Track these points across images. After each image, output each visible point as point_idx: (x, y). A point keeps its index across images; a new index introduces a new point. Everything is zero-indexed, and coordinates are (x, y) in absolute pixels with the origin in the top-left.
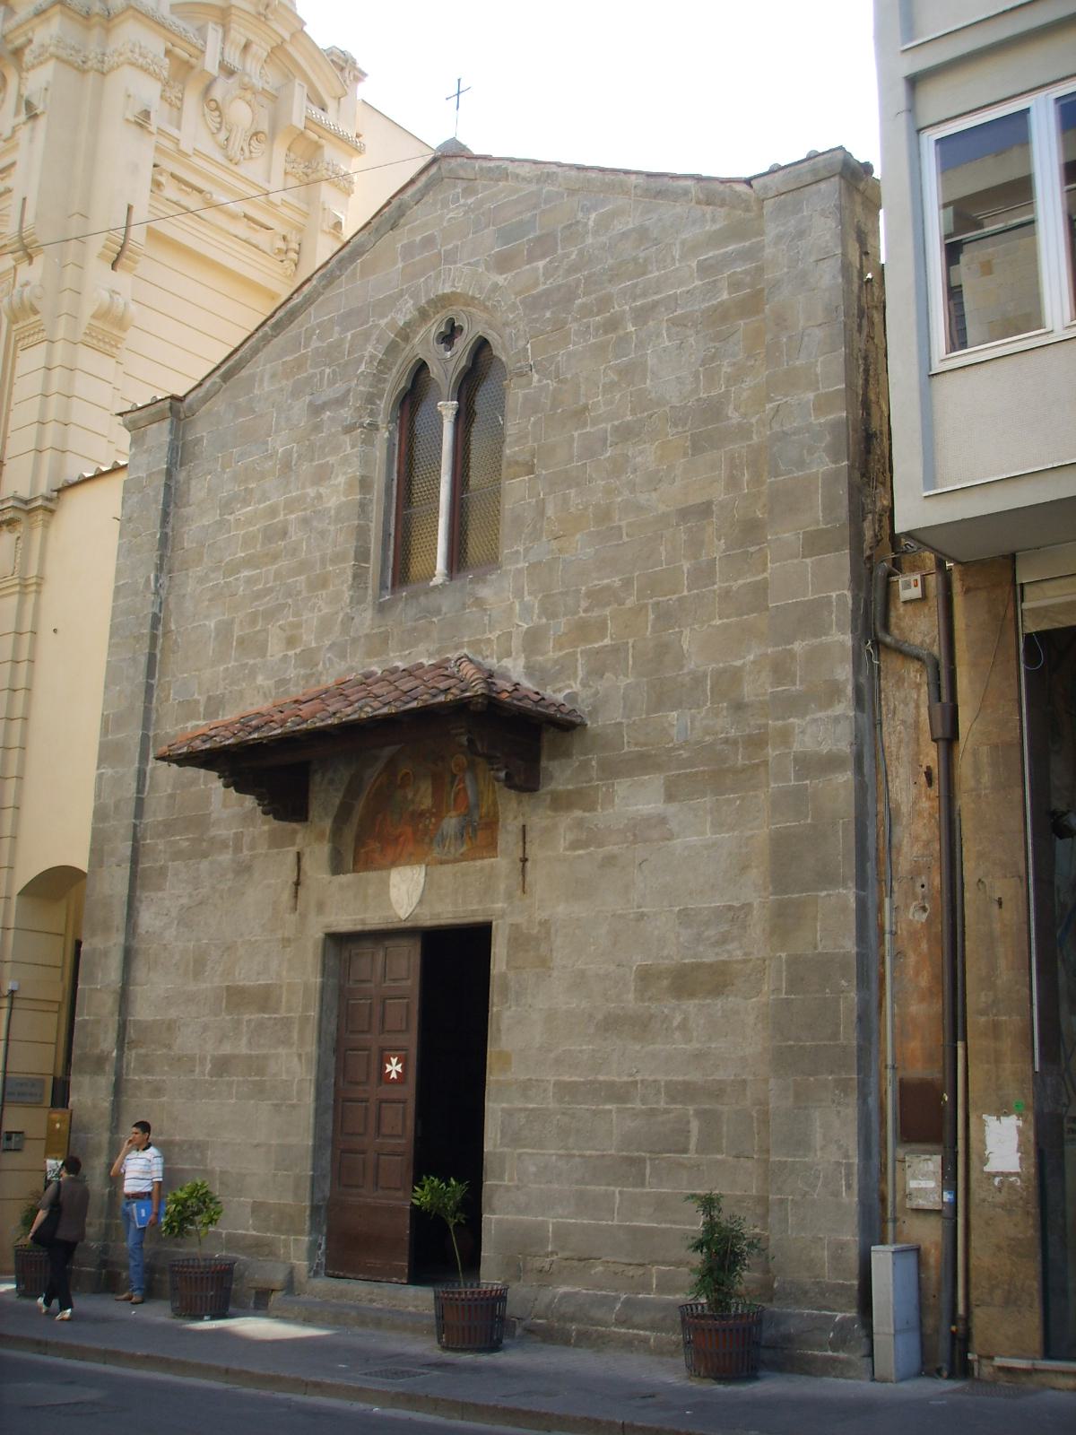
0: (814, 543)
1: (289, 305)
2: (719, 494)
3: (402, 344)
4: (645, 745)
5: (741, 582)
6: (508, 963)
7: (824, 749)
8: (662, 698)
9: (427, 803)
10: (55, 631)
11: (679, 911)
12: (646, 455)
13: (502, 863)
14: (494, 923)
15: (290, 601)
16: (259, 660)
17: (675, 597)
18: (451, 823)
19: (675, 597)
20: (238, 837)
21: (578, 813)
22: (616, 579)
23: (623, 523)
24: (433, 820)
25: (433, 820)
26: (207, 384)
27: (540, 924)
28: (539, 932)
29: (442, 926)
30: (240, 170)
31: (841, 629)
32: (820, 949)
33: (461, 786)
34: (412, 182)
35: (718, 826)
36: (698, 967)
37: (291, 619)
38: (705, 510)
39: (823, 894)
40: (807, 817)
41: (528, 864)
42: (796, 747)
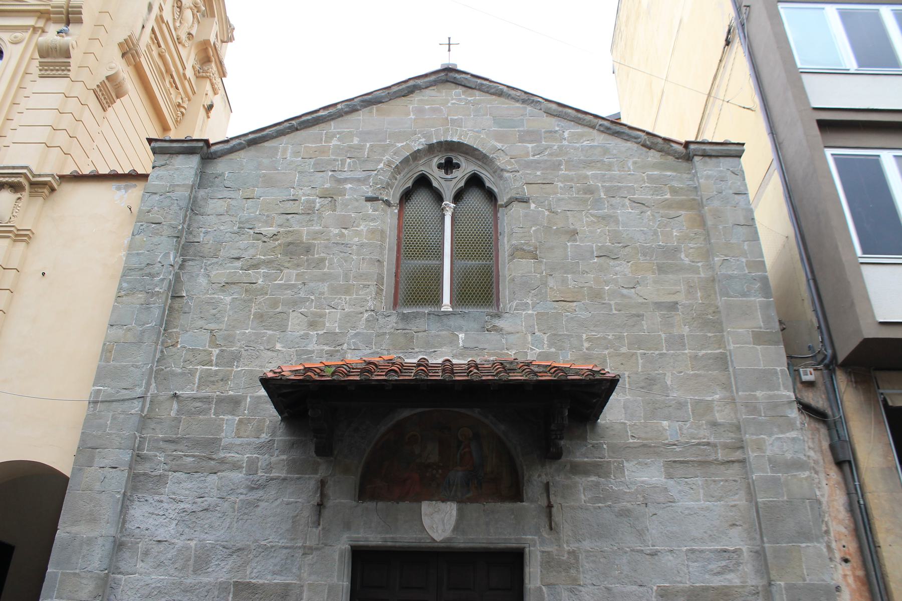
0: (759, 338)
1: (314, 115)
2: (681, 298)
3: (411, 162)
4: (646, 439)
5: (704, 352)
6: (541, 581)
7: (789, 456)
8: (654, 410)
9: (434, 458)
10: (43, 274)
11: (687, 550)
12: (623, 269)
13: (530, 507)
14: (527, 550)
15: (313, 297)
16: (277, 333)
17: (657, 352)
18: (457, 475)
19: (657, 352)
20: (252, 463)
21: (594, 478)
22: (611, 334)
23: (612, 302)
24: (440, 471)
25: (440, 471)
26: (518, 94)
27: (569, 553)
28: (568, 558)
29: (490, 549)
30: (180, 47)
31: (786, 388)
32: (808, 582)
33: (467, 450)
34: (426, 75)
35: (709, 496)
36: (705, 589)
37: (313, 309)
38: (673, 306)
39: (803, 545)
40: (783, 496)
41: (554, 510)
42: (768, 453)
